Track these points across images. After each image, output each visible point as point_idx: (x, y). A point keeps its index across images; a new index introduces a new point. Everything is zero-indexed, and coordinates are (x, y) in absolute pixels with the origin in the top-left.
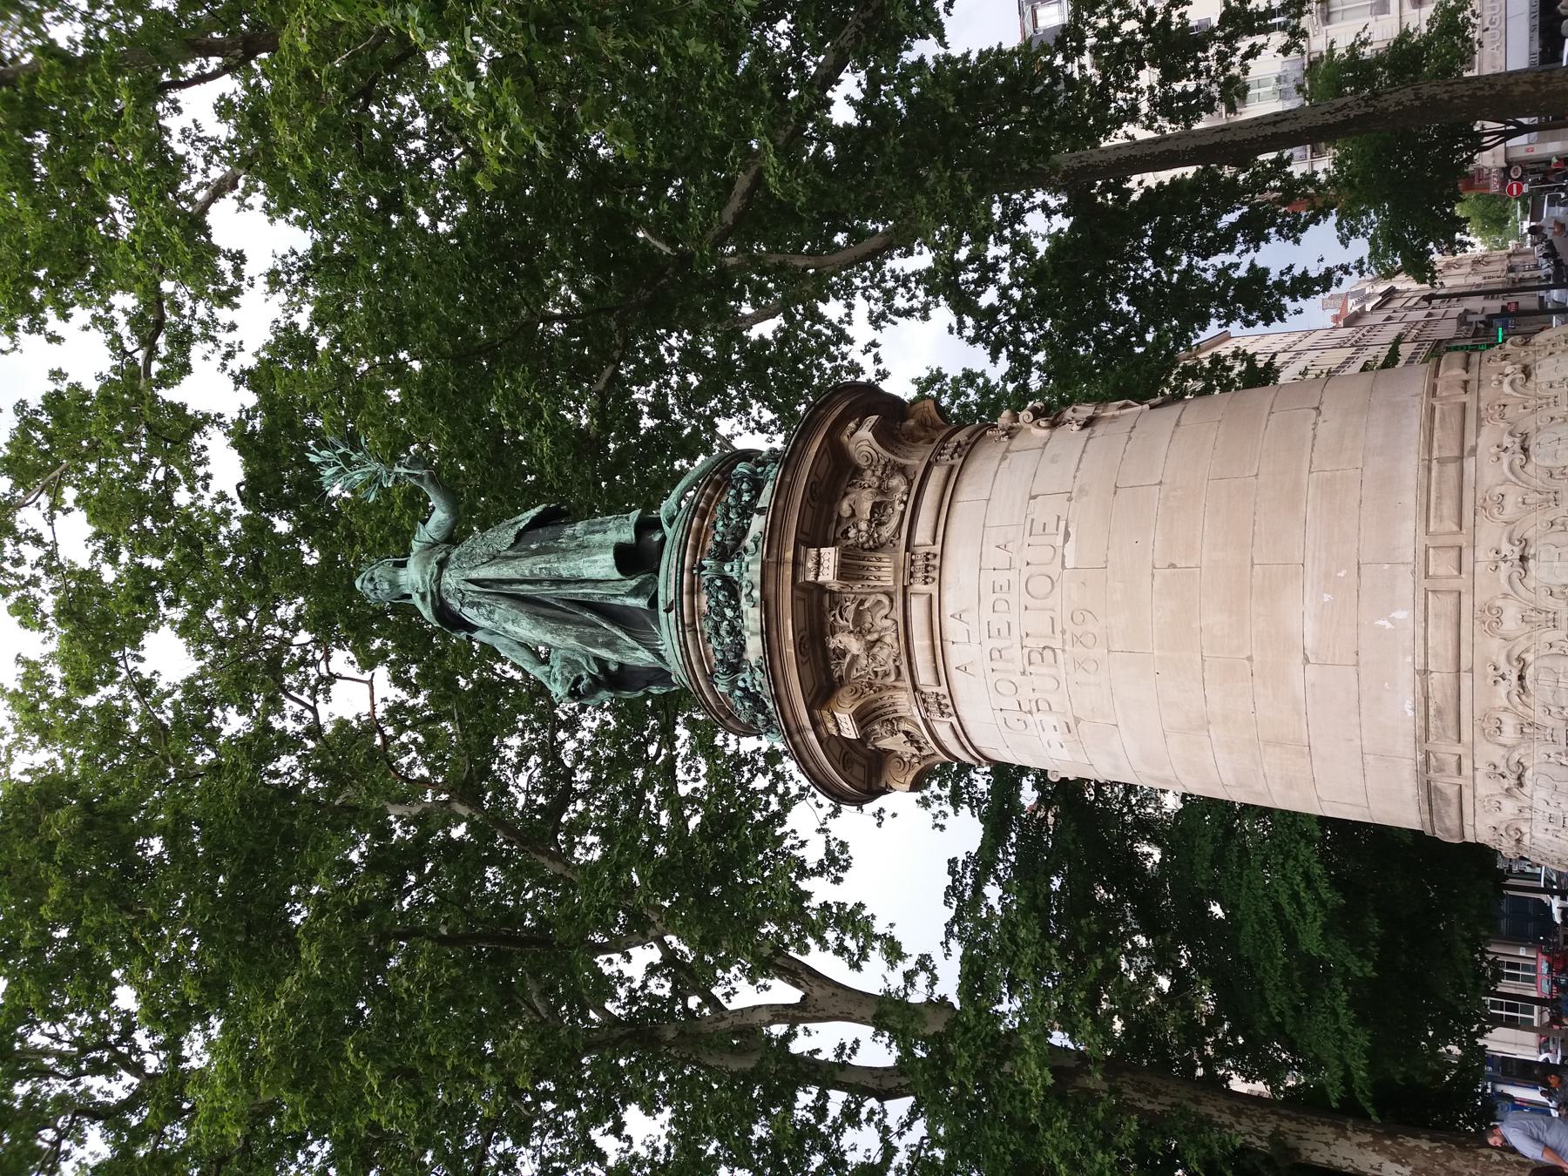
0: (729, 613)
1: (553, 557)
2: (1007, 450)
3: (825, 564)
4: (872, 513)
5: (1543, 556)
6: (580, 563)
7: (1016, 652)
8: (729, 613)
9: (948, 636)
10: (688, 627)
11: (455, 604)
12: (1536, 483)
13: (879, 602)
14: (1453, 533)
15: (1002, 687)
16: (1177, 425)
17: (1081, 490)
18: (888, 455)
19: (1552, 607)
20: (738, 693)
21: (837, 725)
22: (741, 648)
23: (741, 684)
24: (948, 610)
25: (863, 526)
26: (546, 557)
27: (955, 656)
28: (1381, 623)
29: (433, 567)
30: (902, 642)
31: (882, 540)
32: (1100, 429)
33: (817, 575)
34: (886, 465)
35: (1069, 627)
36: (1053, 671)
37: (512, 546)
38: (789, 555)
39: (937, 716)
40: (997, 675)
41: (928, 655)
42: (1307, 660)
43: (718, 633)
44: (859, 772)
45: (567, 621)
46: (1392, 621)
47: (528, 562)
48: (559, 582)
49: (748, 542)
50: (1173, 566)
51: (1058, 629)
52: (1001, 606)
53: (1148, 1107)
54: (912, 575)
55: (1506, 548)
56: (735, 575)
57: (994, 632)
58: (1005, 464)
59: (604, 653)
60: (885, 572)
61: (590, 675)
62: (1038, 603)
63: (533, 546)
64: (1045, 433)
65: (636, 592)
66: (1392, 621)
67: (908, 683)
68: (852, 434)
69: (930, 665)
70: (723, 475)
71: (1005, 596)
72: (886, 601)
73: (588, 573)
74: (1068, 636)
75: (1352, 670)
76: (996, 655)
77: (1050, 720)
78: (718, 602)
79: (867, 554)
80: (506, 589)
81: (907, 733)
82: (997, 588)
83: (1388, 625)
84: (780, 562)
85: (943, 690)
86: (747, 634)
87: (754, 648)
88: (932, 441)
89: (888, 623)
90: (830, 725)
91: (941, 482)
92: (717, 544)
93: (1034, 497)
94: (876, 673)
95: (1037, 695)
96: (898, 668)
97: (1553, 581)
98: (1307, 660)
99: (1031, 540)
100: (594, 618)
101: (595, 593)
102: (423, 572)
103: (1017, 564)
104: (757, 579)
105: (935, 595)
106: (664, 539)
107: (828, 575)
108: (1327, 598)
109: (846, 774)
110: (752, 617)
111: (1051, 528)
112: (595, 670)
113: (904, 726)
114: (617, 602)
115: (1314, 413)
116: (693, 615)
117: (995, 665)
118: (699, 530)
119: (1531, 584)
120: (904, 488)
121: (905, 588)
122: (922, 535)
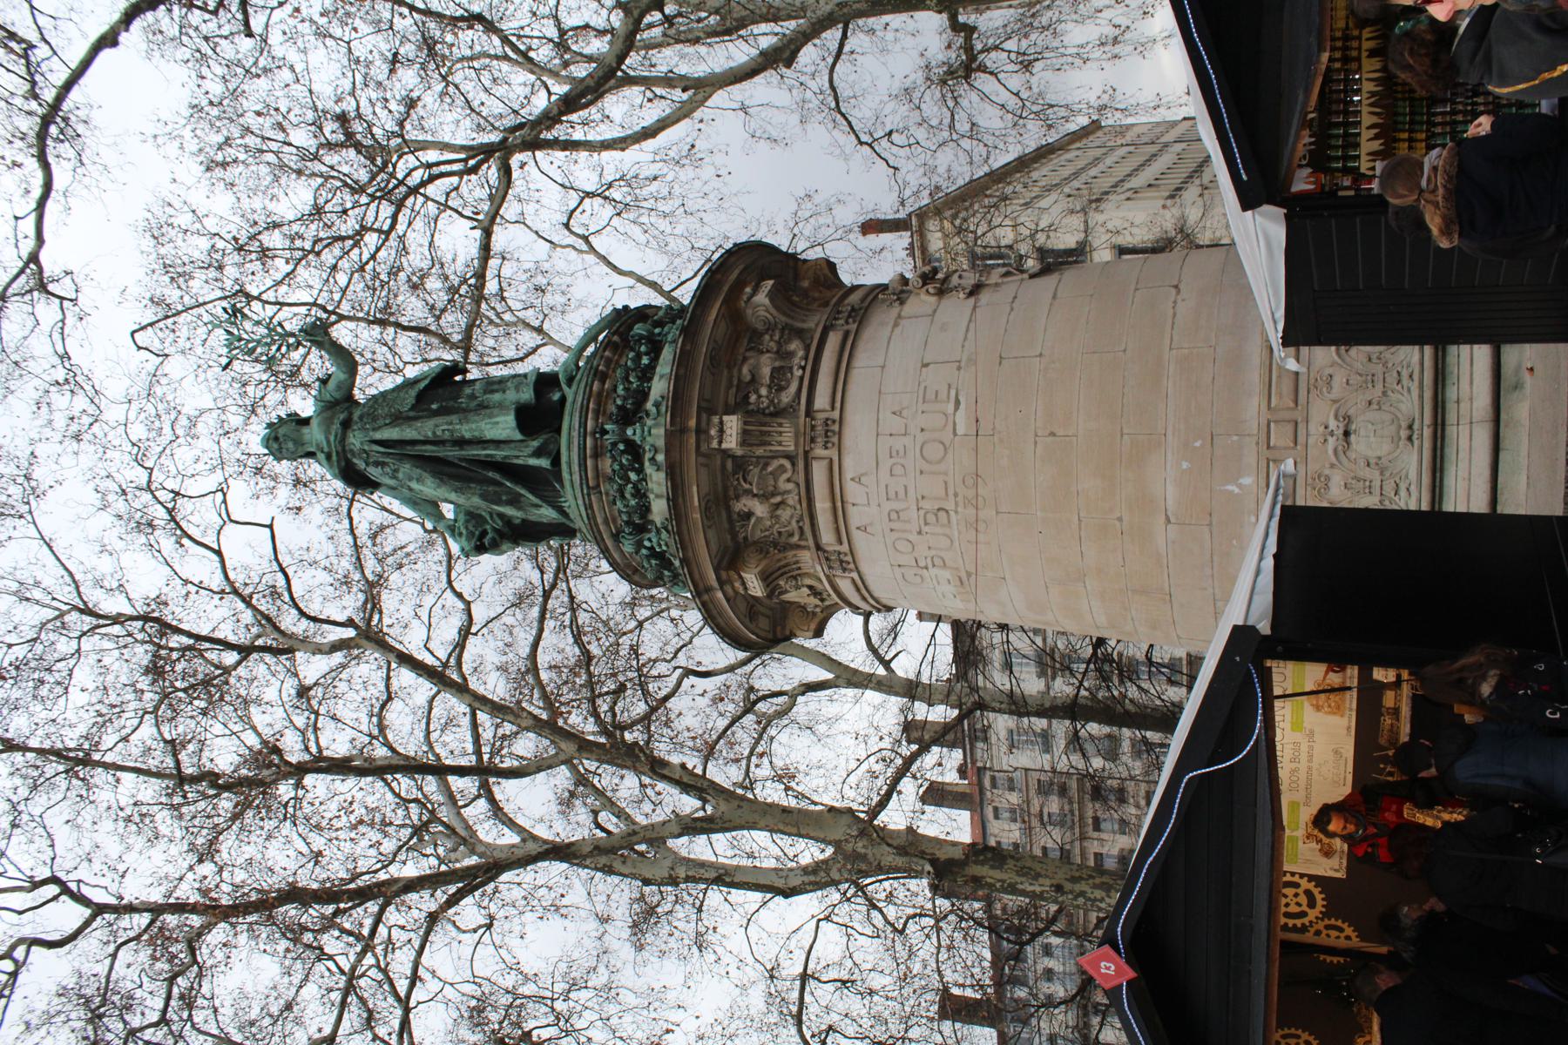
0: (633, 476)
1: (454, 418)
2: (899, 316)
3: (728, 432)
4: (772, 377)
5: (1362, 432)
6: (482, 425)
7: (913, 513)
8: (633, 476)
9: (850, 498)
10: (591, 489)
11: (361, 465)
12: (1358, 366)
14: (1289, 409)
16: (1054, 297)
18: (783, 319)
19: (1368, 476)
20: (644, 551)
21: (744, 584)
22: (645, 509)
23: (647, 544)
24: (849, 474)
25: (764, 391)
26: (448, 419)
27: (856, 517)
28: (1230, 487)
29: (336, 426)
30: (804, 505)
31: (782, 405)
32: (985, 297)
33: (720, 442)
36: (947, 531)
37: (413, 408)
38: (693, 423)
39: (839, 572)
40: (895, 535)
42: (1168, 520)
43: (623, 497)
44: (764, 623)
45: (469, 480)
46: (1240, 486)
47: (431, 423)
48: (461, 443)
49: (649, 405)
50: (1053, 434)
51: (951, 492)
52: (898, 470)
53: (1030, 888)
54: (813, 440)
55: (1333, 424)
56: (637, 439)
57: (892, 494)
58: (898, 331)
59: (509, 511)
60: (786, 437)
61: (495, 530)
63: (434, 406)
64: (933, 299)
65: (538, 453)
66: (1240, 486)
67: (811, 542)
69: (831, 526)
70: (621, 335)
73: (491, 433)
74: (960, 498)
75: (1206, 529)
76: (894, 516)
77: (946, 574)
78: (621, 465)
79: (768, 419)
80: (409, 450)
81: (810, 587)
83: (1237, 490)
84: (684, 430)
85: (845, 548)
86: (652, 496)
87: (659, 509)
88: (826, 304)
89: (790, 486)
90: (737, 584)
92: (619, 407)
93: (926, 365)
95: (933, 552)
96: (801, 528)
97: (1370, 453)
98: (1168, 520)
99: (926, 407)
100: (497, 477)
101: (499, 454)
102: (327, 432)
104: (661, 443)
105: (836, 459)
106: (563, 399)
107: (731, 442)
108: (1185, 465)
109: (752, 626)
110: (657, 481)
111: (943, 395)
112: (499, 524)
113: (808, 581)
114: (520, 462)
115: (1174, 291)
116: (597, 476)
117: (894, 525)
118: (600, 394)
119: (1353, 455)
120: (801, 353)
121: (806, 453)
122: (821, 401)
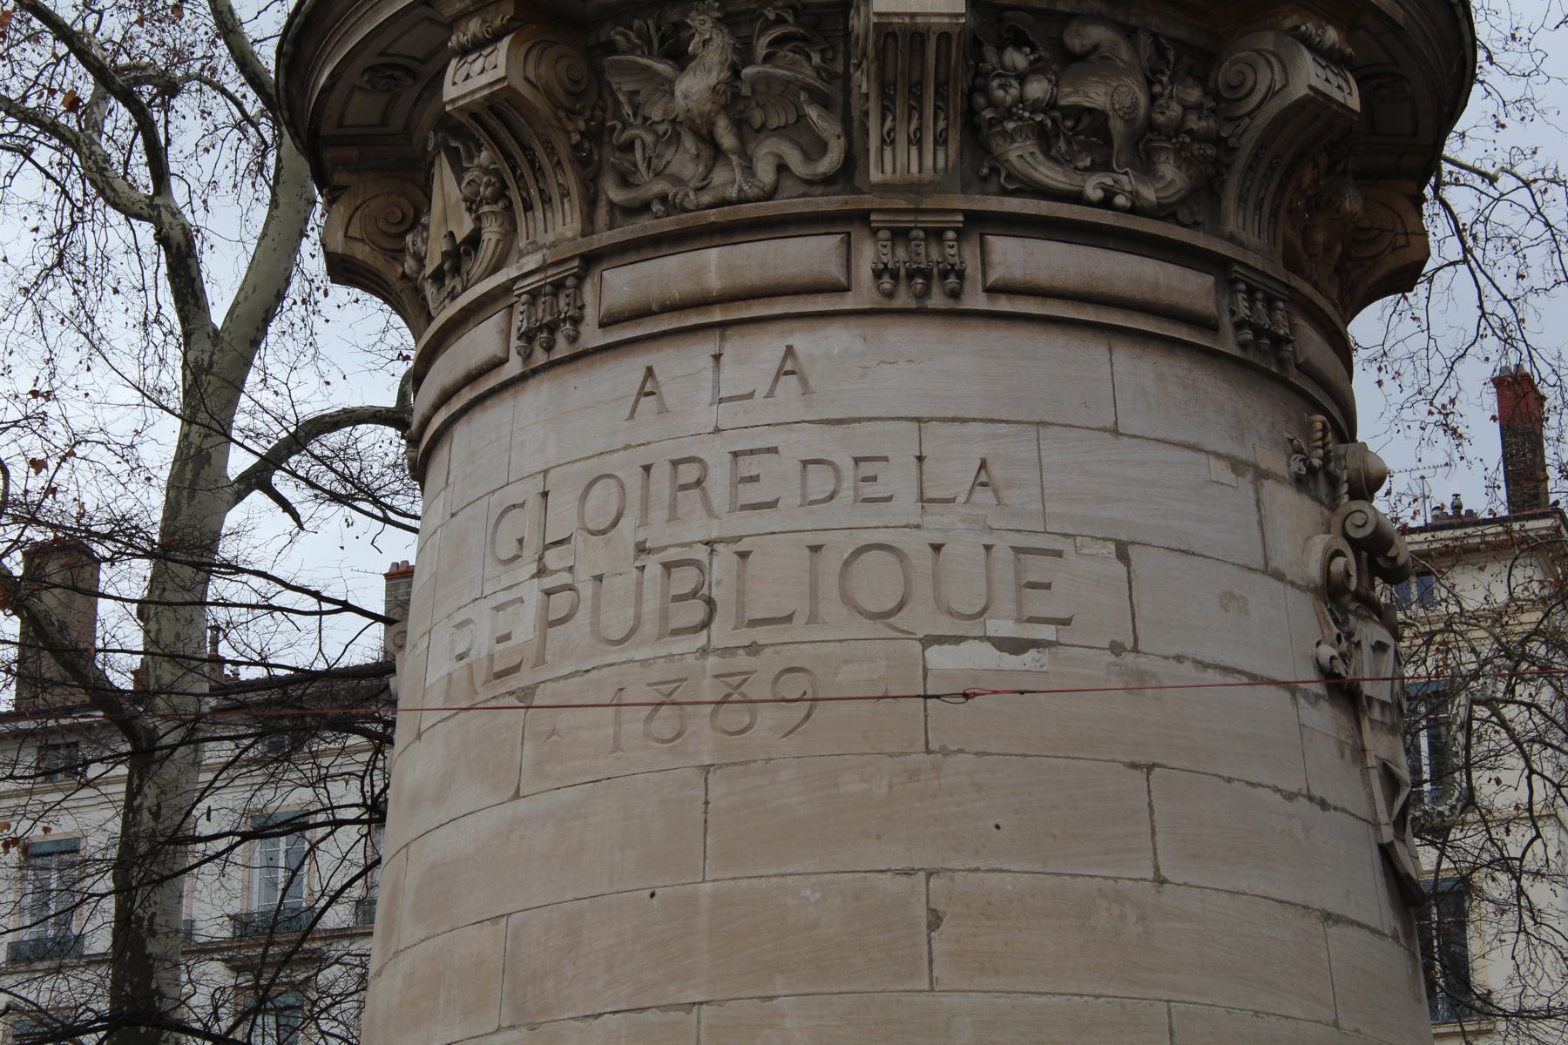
2: (1261, 475)
4: (1078, 112)
7: (697, 528)
9: (734, 346)
13: (823, 148)
15: (603, 500)
17: (1141, 675)
18: (1248, 143)
21: (478, 45)
24: (805, 341)
25: (1037, 89)
27: (680, 366)
30: (713, 216)
31: (998, 145)
32: (1324, 719)
34: (1218, 141)
35: (767, 665)
36: (649, 627)
40: (634, 481)
41: (678, 289)
44: (363, 109)
51: (761, 635)
52: (820, 483)
54: (900, 235)
57: (748, 466)
58: (1221, 471)
60: (901, 160)
62: (829, 581)
64: (1314, 571)
67: (605, 238)
68: (1306, 40)
71: (847, 492)
72: (826, 165)
74: (743, 661)
77: (525, 629)
79: (956, 104)
81: (474, 240)
82: (867, 469)
85: (592, 336)
88: (1292, 264)
90: (474, 27)
91: (1167, 298)
93: (1122, 554)
94: (629, 147)
95: (586, 590)
96: (644, 208)
99: (1002, 553)
103: (936, 519)
105: (848, 302)
111: (1038, 604)
113: (491, 233)
117: (661, 474)
120: (1149, 194)
121: (862, 217)
122: (1013, 256)
